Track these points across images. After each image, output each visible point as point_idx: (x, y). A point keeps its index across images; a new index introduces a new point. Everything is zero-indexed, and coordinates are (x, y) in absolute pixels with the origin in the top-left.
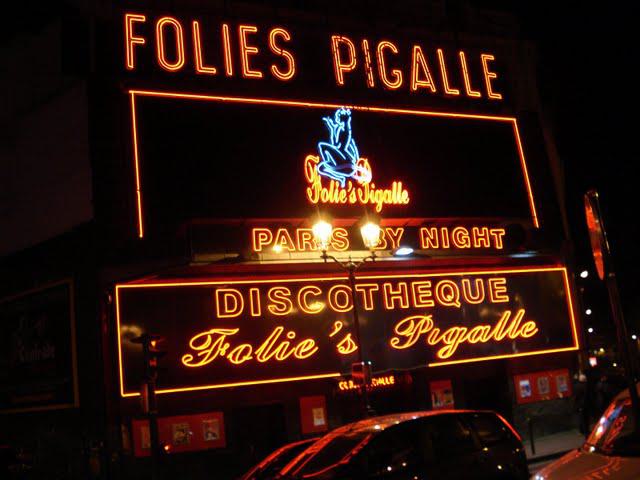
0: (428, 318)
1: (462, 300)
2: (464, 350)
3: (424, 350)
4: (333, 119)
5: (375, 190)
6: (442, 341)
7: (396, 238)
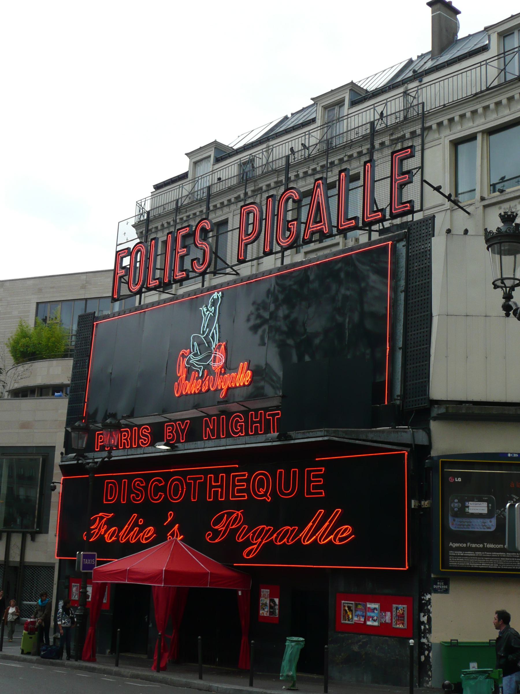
1: (274, 494)
2: (269, 551)
4: (207, 306)
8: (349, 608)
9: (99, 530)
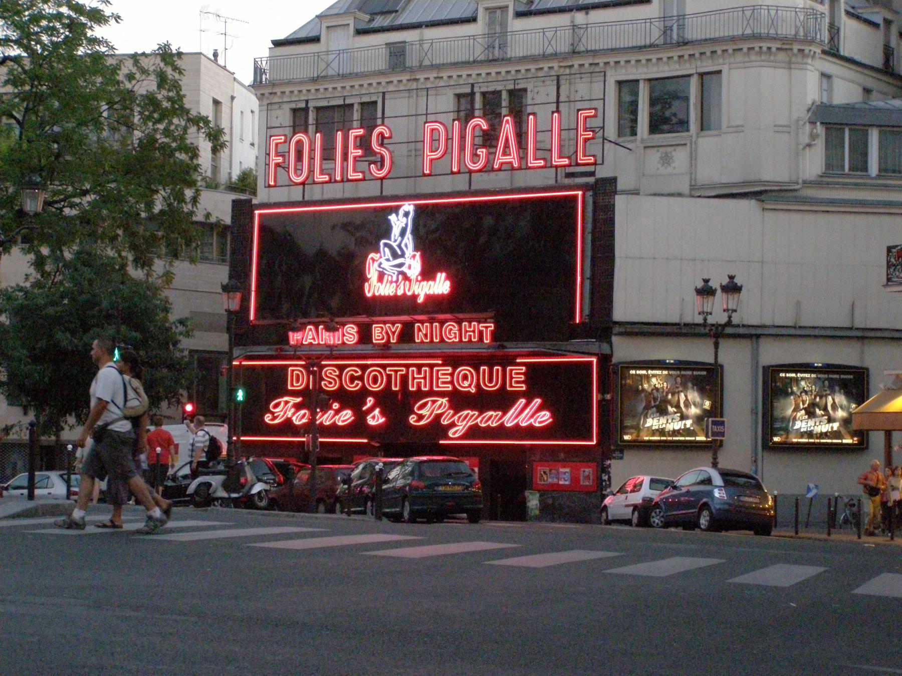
0: (444, 400)
1: (478, 385)
2: (474, 432)
3: (437, 428)
5: (420, 281)
6: (454, 422)
7: (394, 333)
8: (545, 472)
9: (285, 413)
